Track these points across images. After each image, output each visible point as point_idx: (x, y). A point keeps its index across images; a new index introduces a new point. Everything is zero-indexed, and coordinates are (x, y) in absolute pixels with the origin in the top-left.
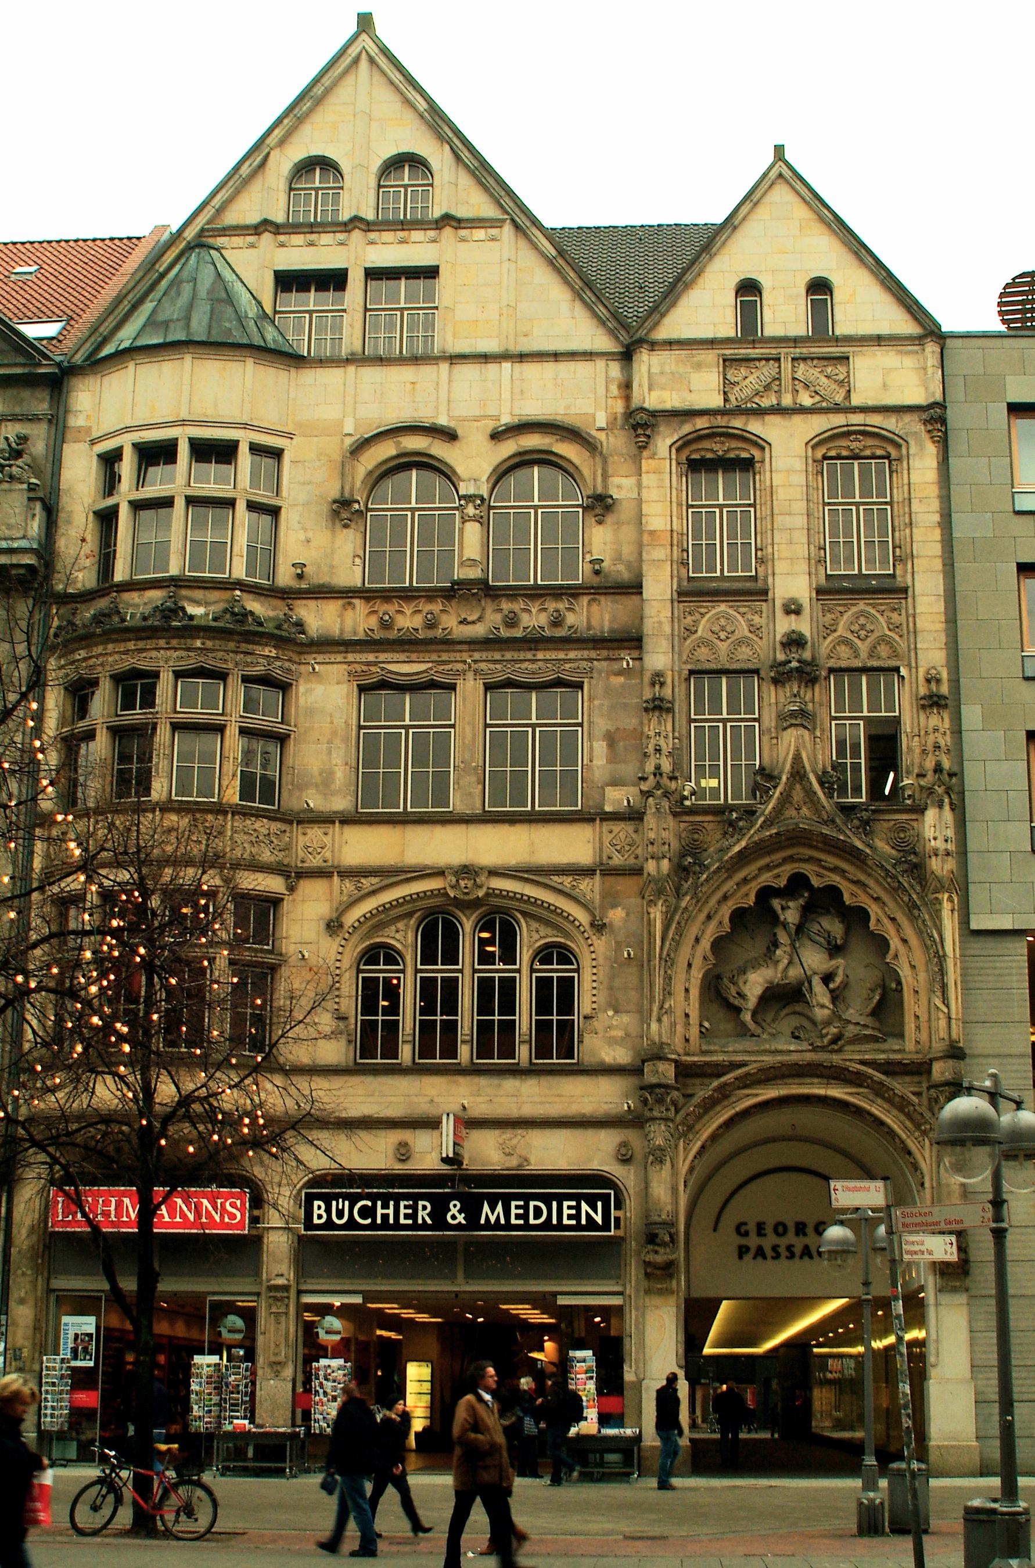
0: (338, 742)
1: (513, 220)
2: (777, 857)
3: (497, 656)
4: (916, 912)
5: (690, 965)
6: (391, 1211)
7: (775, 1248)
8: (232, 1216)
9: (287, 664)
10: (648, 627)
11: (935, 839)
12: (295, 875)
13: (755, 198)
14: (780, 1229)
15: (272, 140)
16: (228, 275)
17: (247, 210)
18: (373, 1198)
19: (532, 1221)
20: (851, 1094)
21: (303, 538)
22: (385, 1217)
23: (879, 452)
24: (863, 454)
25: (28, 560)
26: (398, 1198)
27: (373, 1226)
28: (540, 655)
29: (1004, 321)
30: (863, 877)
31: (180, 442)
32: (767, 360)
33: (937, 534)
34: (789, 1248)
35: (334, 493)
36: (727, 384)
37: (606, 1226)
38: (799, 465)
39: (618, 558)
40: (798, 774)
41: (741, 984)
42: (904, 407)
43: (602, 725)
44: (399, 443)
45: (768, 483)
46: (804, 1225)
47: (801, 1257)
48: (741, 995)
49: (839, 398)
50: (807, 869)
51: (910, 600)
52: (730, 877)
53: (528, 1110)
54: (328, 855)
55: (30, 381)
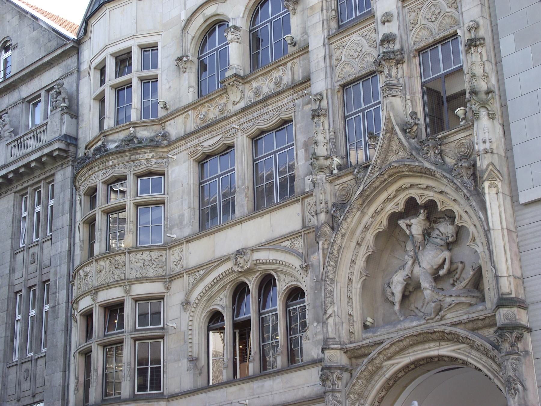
0: (186, 197)
2: (392, 190)
3: (251, 117)
5: (350, 280)
9: (160, 160)
12: (169, 279)
20: (454, 351)
21: (168, 87)
25: (56, 146)
28: (270, 108)
30: (443, 188)
44: (204, 14)
50: (413, 193)
52: (363, 213)
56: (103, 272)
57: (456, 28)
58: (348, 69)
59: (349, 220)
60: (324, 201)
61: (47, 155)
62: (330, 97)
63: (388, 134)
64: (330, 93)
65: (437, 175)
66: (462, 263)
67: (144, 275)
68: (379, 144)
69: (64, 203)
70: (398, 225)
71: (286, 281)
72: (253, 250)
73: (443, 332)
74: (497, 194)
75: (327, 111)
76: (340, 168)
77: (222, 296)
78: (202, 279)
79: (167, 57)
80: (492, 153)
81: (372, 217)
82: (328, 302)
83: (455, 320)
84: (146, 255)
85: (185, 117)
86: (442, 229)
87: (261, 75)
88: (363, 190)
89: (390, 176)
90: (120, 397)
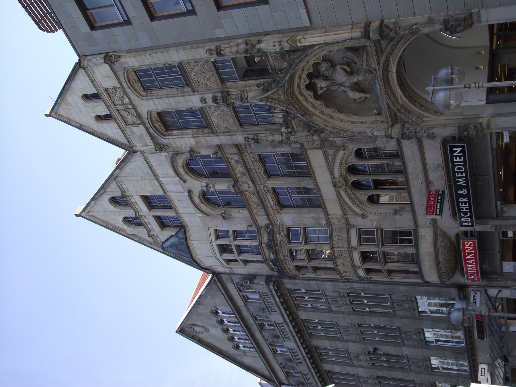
2: (301, 98)
3: (257, 178)
5: (352, 122)
6: (464, 208)
8: (471, 244)
12: (349, 226)
13: (68, 121)
19: (463, 170)
23: (133, 74)
24: (137, 79)
28: (252, 167)
32: (120, 113)
36: (134, 124)
37: (463, 147)
38: (151, 102)
50: (303, 86)
52: (314, 114)
53: (419, 164)
57: (210, 62)
58: (231, 123)
59: (317, 123)
61: (276, 293)
62: (247, 133)
65: (293, 72)
66: (343, 58)
70: (321, 94)
72: (333, 177)
75: (254, 135)
76: (287, 128)
78: (349, 207)
80: (281, 41)
83: (376, 63)
84: (335, 238)
86: (324, 69)
89: (293, 99)
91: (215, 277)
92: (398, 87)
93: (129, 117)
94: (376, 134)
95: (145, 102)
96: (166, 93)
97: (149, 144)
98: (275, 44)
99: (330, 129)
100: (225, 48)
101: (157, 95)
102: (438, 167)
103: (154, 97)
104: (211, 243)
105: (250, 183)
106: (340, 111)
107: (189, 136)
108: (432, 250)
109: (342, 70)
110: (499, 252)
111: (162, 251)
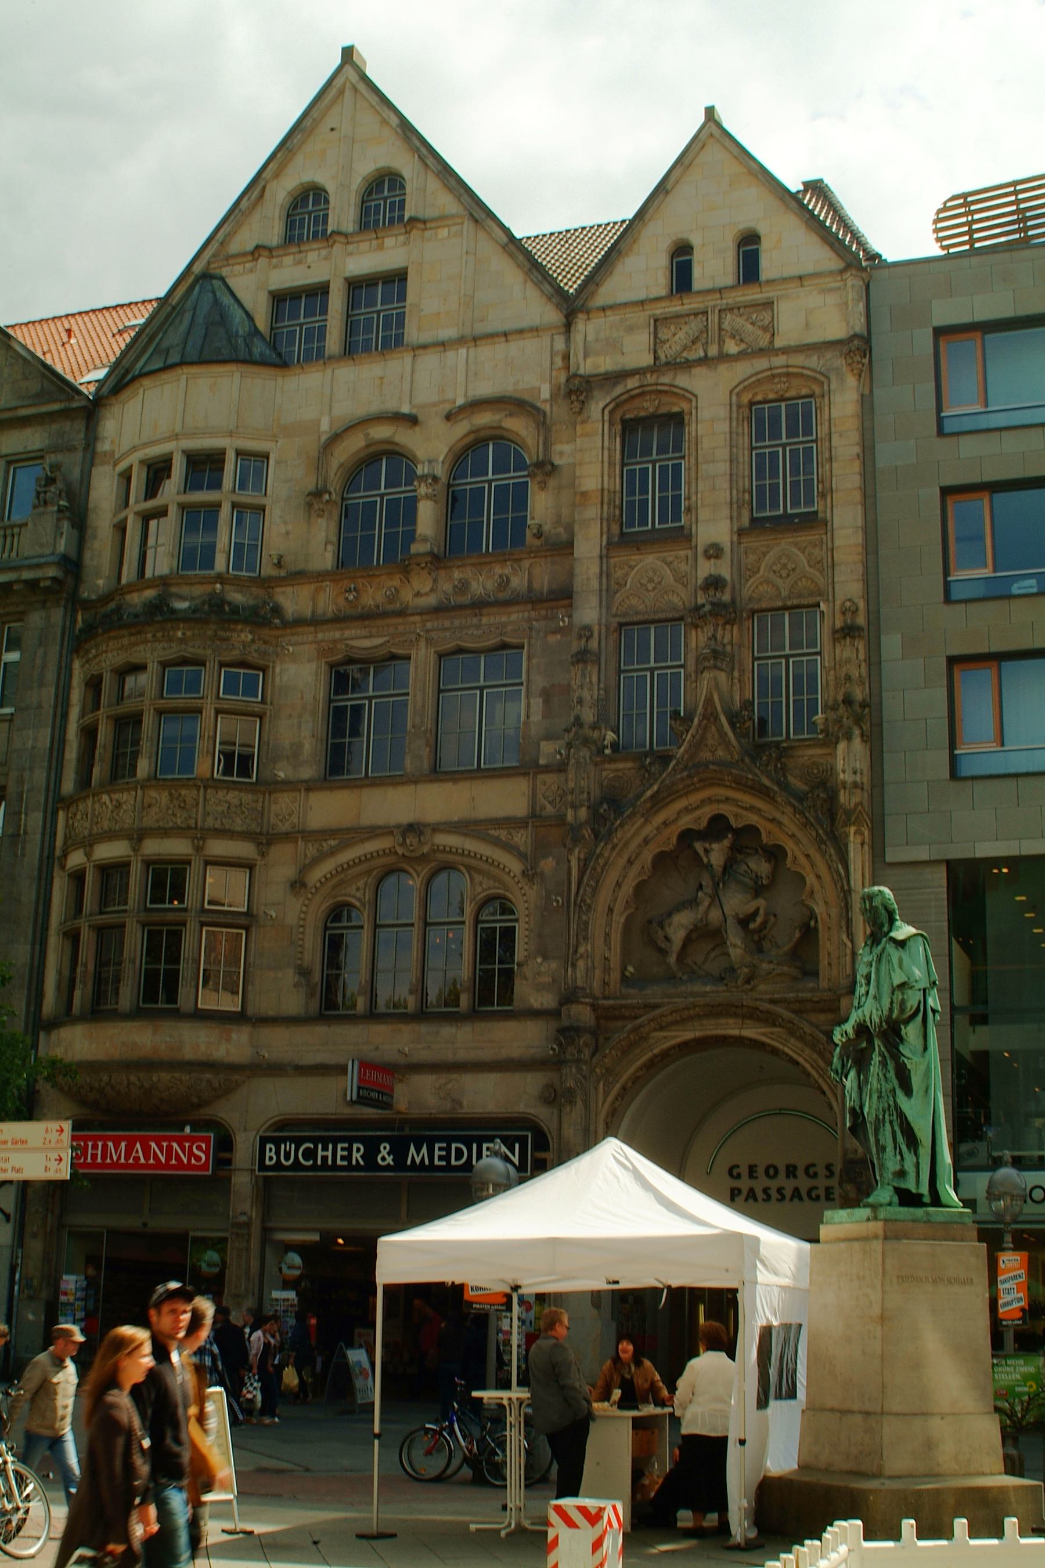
1: (471, 215)
2: (695, 798)
4: (823, 846)
5: (611, 910)
6: (329, 1154)
7: (765, 1191)
10: (577, 585)
11: (844, 772)
13: (686, 162)
14: (771, 1171)
15: (267, 174)
16: (227, 300)
17: (245, 239)
18: (315, 1140)
20: (764, 1034)
21: (283, 531)
22: (325, 1158)
23: (804, 392)
24: (787, 395)
26: (335, 1141)
27: (314, 1167)
29: (943, 248)
30: (778, 815)
31: (175, 454)
32: (696, 315)
33: (857, 467)
34: (779, 1190)
35: (311, 487)
36: (657, 342)
38: (723, 413)
39: (558, 521)
40: (710, 716)
41: (666, 928)
42: (824, 343)
43: (539, 682)
45: (694, 434)
46: (795, 1167)
47: (791, 1199)
48: (667, 938)
49: (764, 341)
50: (725, 809)
51: (829, 534)
54: (296, 821)
55: (65, 414)
56: (155, 809)
57: (818, 599)
58: (634, 601)
59: (627, 827)
60: (586, 790)
61: (26, 582)
62: (603, 637)
63: (705, 722)
64: (603, 631)
65: (779, 799)
66: (775, 916)
67: (227, 827)
68: (690, 732)
69: (44, 666)
70: (690, 846)
71: (484, 886)
73: (757, 1009)
74: (862, 844)
75: (598, 656)
76: (615, 746)
77: (361, 884)
78: (333, 852)
79: (286, 481)
80: (862, 789)
81: (658, 829)
82: (580, 937)
85: (316, 590)
86: (753, 865)
87: (474, 565)
88: (657, 792)
89: (700, 781)
90: (178, 1009)
91: (84, 403)
92: (698, 1034)
93: (681, 335)
94: (581, 964)
95: (722, 394)
96: (741, 460)
97: (589, 361)
98: (858, 774)
99: (606, 855)
100: (857, 650)
101: (737, 434)
102: (453, 1100)
103: (734, 424)
104: (176, 437)
105: (432, 600)
106: (639, 888)
107: (606, 478)
108: (188, 1054)
109: (752, 910)
110: (145, 1225)
111: (197, 269)
